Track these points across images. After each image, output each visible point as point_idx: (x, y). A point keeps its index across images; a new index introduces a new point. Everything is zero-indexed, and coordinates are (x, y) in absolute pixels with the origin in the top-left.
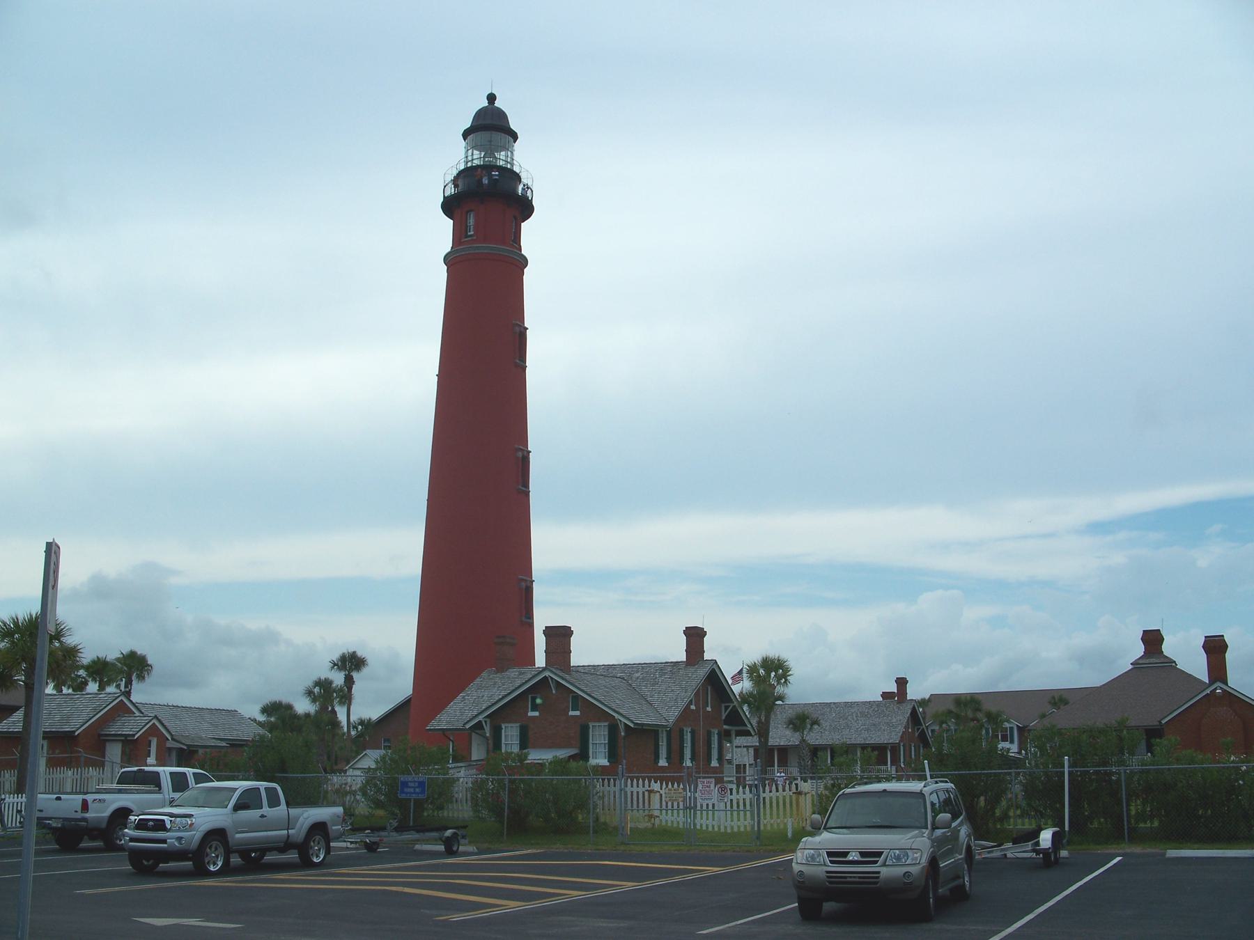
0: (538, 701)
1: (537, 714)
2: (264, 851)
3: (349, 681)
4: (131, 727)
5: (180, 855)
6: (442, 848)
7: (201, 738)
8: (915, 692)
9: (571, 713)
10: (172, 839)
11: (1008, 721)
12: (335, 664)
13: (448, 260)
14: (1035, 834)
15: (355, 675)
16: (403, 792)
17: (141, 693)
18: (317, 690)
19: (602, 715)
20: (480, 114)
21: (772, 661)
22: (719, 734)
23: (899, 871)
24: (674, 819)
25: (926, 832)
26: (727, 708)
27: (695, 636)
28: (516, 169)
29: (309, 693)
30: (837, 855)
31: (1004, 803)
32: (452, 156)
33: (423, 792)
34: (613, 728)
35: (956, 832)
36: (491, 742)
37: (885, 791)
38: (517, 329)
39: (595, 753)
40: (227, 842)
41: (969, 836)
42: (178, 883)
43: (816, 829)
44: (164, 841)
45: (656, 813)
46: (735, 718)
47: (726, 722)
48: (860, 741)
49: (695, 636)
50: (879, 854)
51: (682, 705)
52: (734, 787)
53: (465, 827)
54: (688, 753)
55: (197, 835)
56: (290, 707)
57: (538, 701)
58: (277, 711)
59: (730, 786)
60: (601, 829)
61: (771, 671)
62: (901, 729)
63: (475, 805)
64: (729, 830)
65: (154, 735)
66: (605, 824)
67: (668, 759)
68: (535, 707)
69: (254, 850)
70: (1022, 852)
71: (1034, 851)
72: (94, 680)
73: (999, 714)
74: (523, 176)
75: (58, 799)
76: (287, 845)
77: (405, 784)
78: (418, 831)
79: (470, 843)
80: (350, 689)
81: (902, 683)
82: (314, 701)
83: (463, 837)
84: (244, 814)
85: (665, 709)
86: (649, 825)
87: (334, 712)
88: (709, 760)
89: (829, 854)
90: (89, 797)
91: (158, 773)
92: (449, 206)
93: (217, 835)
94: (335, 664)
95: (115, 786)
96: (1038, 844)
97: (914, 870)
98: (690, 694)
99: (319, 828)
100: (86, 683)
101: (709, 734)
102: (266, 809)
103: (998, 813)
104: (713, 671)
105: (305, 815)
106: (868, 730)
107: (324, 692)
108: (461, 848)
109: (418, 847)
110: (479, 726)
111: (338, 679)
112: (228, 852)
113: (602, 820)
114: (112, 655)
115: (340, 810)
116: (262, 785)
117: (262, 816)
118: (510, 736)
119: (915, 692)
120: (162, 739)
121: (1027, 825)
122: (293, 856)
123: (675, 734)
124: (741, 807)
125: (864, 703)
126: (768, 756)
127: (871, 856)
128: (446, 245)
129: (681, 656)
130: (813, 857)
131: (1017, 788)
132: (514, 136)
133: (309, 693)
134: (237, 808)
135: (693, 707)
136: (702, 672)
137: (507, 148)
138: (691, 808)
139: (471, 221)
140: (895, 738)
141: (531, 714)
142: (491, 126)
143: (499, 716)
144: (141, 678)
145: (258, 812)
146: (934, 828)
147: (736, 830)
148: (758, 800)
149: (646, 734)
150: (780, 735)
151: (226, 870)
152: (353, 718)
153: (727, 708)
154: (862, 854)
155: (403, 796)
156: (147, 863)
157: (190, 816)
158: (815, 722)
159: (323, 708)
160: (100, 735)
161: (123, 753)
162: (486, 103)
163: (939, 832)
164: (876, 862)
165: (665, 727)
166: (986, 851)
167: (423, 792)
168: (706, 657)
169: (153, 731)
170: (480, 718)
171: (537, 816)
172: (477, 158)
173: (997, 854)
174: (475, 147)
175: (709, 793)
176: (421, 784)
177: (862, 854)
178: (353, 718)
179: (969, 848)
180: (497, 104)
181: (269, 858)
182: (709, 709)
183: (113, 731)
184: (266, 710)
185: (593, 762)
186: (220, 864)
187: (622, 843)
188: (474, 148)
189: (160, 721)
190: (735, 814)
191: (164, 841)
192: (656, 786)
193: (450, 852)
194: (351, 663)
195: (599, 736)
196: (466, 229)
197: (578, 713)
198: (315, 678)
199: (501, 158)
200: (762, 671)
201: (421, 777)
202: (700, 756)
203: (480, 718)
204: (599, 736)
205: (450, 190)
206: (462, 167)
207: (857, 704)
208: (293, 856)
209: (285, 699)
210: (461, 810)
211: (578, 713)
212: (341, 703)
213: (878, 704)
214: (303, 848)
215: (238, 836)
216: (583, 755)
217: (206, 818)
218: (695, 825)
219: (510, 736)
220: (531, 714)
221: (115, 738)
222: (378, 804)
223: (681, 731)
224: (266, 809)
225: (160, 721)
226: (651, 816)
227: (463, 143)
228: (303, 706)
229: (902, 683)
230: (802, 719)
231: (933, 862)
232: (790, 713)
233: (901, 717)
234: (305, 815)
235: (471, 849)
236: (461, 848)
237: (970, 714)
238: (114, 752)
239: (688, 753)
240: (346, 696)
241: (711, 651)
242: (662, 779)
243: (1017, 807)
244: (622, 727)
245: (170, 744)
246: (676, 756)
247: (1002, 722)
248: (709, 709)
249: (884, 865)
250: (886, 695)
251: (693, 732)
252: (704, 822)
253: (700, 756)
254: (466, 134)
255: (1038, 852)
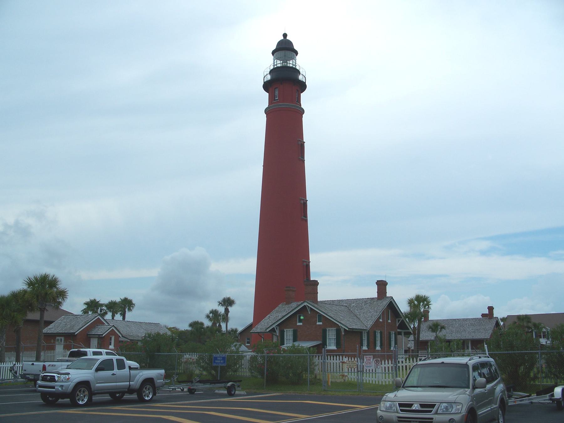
0: (302, 318)
1: (301, 324)
2: (123, 393)
3: (227, 311)
4: (101, 331)
5: (63, 395)
6: (226, 392)
7: (138, 336)
8: (499, 313)
9: (318, 323)
10: (58, 387)
11: (544, 328)
12: (220, 303)
13: (267, 111)
14: (551, 389)
15: (230, 308)
16: (215, 363)
17: (129, 316)
18: (211, 315)
19: (333, 324)
20: (280, 43)
21: (422, 297)
22: (395, 334)
23: (447, 418)
24: (352, 377)
25: (468, 391)
26: (399, 321)
27: (382, 285)
28: (297, 68)
29: (208, 317)
30: (405, 406)
31: (535, 370)
32: (266, 63)
33: (224, 362)
34: (338, 331)
35: (493, 390)
36: (279, 338)
37: (443, 363)
38: (300, 143)
39: (330, 343)
40: (91, 388)
41: (502, 392)
42: (46, 412)
43: (398, 386)
44: (53, 387)
45: (346, 374)
46: (403, 326)
47: (399, 328)
48: (470, 337)
49: (382, 285)
50: (433, 406)
51: (374, 319)
52: (404, 360)
53: (241, 381)
54: (378, 343)
55: (71, 385)
56: (202, 324)
57: (302, 318)
58: (196, 325)
59: (402, 360)
60: (316, 382)
61: (420, 302)
62: (490, 332)
63: (250, 370)
64: (384, 384)
65: (113, 335)
66: (319, 379)
67: (368, 346)
68: (300, 321)
69: (119, 393)
70: (545, 399)
71: (550, 399)
72: (110, 311)
73: (540, 324)
74: (301, 71)
75: (33, 364)
76: (130, 390)
77: (216, 358)
78: (211, 383)
79: (243, 389)
80: (227, 315)
81: (491, 309)
82: (210, 320)
83: (239, 386)
84: (101, 373)
85: (366, 321)
86: (343, 381)
87: (220, 326)
88: (390, 345)
89: (400, 405)
90: (47, 364)
91: (86, 352)
92: (267, 86)
93: (84, 385)
94: (220, 303)
95: (67, 358)
96: (553, 395)
97: (457, 417)
98: (379, 314)
99: (149, 381)
100: (106, 313)
101: (390, 334)
102: (116, 371)
103: (532, 375)
104: (391, 302)
105: (141, 374)
106: (474, 332)
107: (214, 316)
108: (237, 392)
109: (217, 391)
110: (273, 330)
111: (221, 310)
112: (92, 394)
113: (318, 377)
114: (118, 300)
115: (162, 372)
116: (115, 358)
117: (113, 374)
118: (289, 334)
119: (499, 313)
120: (117, 337)
121: (549, 382)
122: (134, 396)
123: (371, 334)
124: (387, 371)
125: (473, 319)
126: (422, 345)
127: (427, 406)
128: (266, 105)
129: (375, 295)
130: (391, 407)
131: (543, 362)
132: (296, 53)
133: (208, 317)
134: (97, 370)
135: (381, 320)
136: (385, 303)
137: (293, 58)
138: (361, 371)
139: (277, 93)
140: (487, 336)
141: (298, 324)
142: (285, 48)
143: (283, 324)
144: (130, 310)
145: (111, 372)
146: (474, 388)
147: (387, 383)
148: (396, 367)
149: (356, 334)
150: (426, 335)
151: (90, 403)
152: (229, 328)
153: (399, 321)
154: (422, 406)
155: (215, 365)
156: (52, 399)
157: (68, 374)
158: (443, 327)
159: (214, 324)
160: (88, 335)
161: (98, 343)
162: (282, 38)
163: (478, 391)
164: (431, 411)
165: (366, 330)
166: (518, 399)
167: (224, 362)
168: (388, 295)
169: (112, 333)
170: (274, 326)
171: (281, 375)
172: (279, 63)
173: (526, 401)
174: (278, 59)
175: (370, 363)
176: (224, 358)
177: (422, 406)
178: (229, 328)
179: (502, 400)
180: (288, 38)
181: (126, 396)
182: (389, 321)
183: (93, 333)
184: (191, 325)
185: (329, 348)
186: (86, 400)
187: (325, 390)
188: (277, 59)
189: (115, 328)
190: (371, 374)
191: (53, 387)
192: (345, 360)
193: (230, 394)
194: (228, 302)
195: (331, 335)
196: (275, 97)
197: (321, 323)
198: (211, 309)
199: (290, 64)
200: (416, 302)
201: (223, 355)
202: (385, 344)
203: (274, 326)
204: (331, 335)
205: (269, 77)
206: (272, 68)
207: (469, 319)
208: (134, 396)
209: (200, 320)
210: (245, 371)
211: (321, 323)
212: (223, 321)
213: (479, 319)
214: (139, 391)
215: (97, 385)
216: (324, 344)
217: (78, 375)
218: (363, 380)
219: (289, 334)
220: (298, 324)
221: (94, 336)
222: (205, 369)
223: (375, 333)
224: (116, 371)
225: (115, 328)
226: (343, 376)
227: (272, 57)
228: (207, 323)
229: (491, 309)
230: (436, 326)
231: (472, 412)
232: (431, 324)
233: (490, 326)
234: (141, 374)
235: (242, 393)
236: (237, 392)
237: (525, 324)
238: (94, 342)
239: (378, 343)
240: (225, 318)
241: (390, 292)
242: (348, 356)
243: (542, 372)
244: (342, 330)
245: (122, 339)
246: (372, 344)
247: (542, 328)
248: (389, 321)
249: (436, 413)
250: (483, 315)
251: (381, 333)
252: (368, 379)
253: (385, 344)
254: (273, 53)
255: (553, 400)
